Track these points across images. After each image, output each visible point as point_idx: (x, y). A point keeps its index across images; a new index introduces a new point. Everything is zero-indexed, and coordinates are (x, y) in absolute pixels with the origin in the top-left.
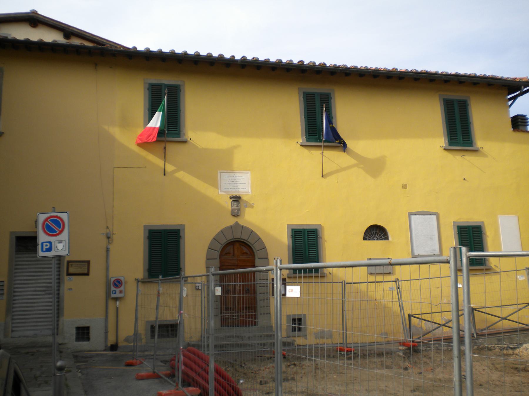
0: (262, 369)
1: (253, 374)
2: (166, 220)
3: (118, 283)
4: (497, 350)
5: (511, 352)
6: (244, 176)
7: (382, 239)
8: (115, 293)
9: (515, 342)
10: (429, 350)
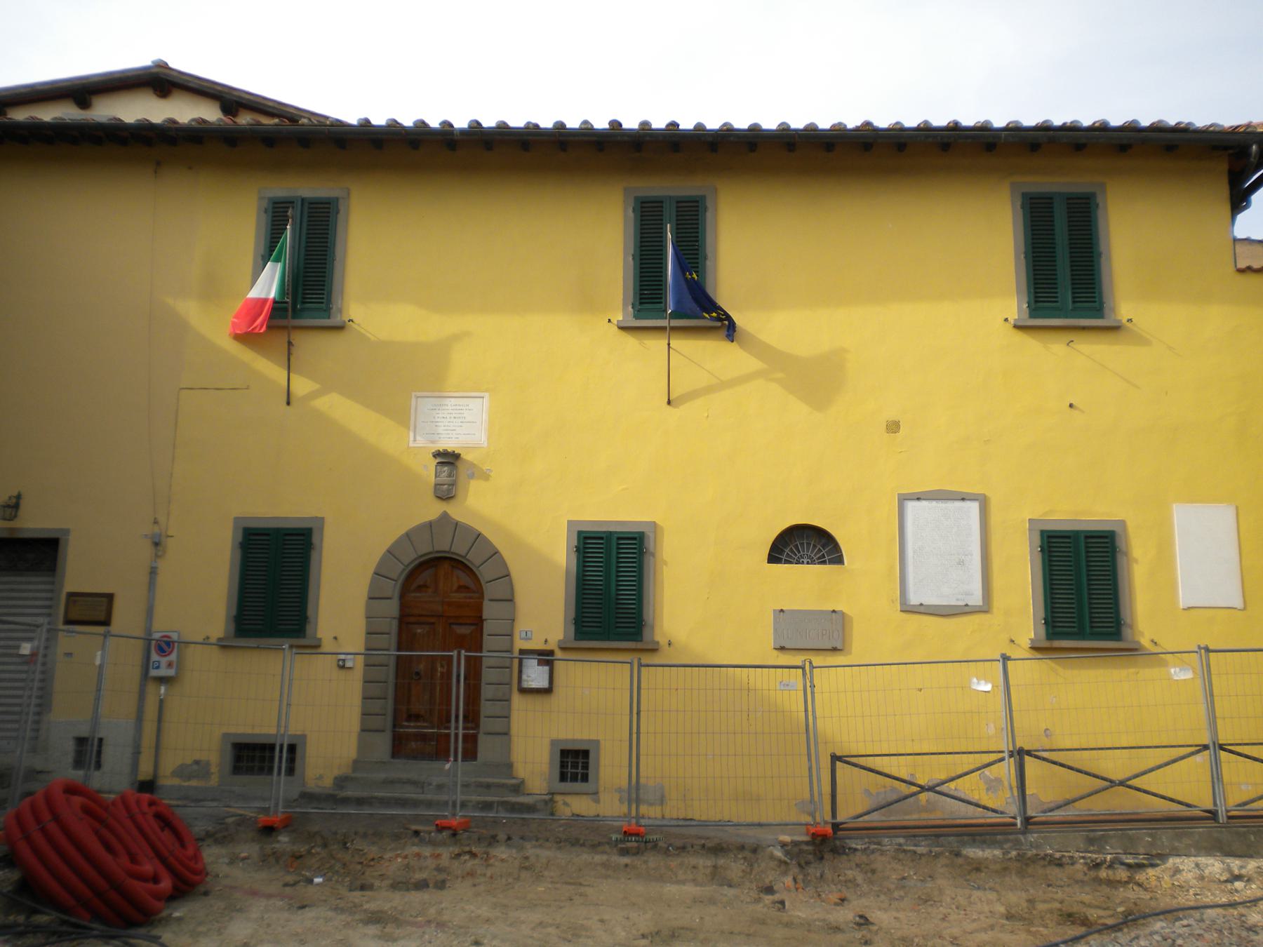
0: (387, 856)
1: (359, 867)
2: (282, 506)
3: (165, 646)
4: (1080, 866)
5: (1122, 874)
6: (474, 404)
7: (824, 563)
8: (158, 667)
9: (1142, 850)
10: (873, 852)
